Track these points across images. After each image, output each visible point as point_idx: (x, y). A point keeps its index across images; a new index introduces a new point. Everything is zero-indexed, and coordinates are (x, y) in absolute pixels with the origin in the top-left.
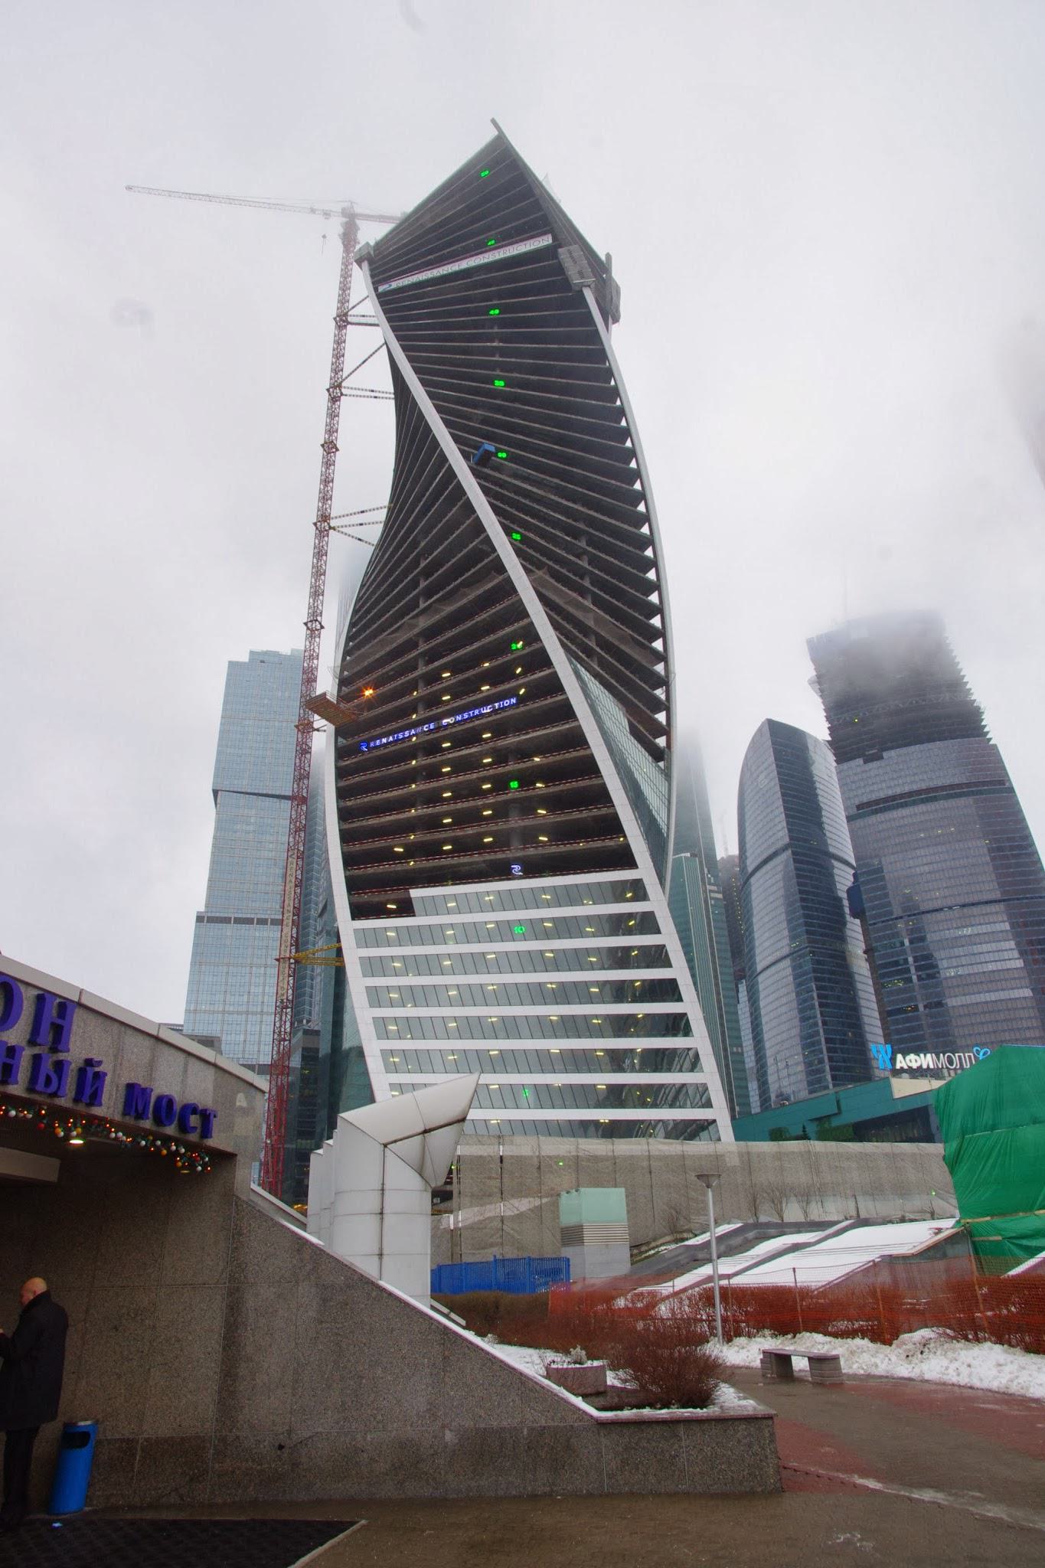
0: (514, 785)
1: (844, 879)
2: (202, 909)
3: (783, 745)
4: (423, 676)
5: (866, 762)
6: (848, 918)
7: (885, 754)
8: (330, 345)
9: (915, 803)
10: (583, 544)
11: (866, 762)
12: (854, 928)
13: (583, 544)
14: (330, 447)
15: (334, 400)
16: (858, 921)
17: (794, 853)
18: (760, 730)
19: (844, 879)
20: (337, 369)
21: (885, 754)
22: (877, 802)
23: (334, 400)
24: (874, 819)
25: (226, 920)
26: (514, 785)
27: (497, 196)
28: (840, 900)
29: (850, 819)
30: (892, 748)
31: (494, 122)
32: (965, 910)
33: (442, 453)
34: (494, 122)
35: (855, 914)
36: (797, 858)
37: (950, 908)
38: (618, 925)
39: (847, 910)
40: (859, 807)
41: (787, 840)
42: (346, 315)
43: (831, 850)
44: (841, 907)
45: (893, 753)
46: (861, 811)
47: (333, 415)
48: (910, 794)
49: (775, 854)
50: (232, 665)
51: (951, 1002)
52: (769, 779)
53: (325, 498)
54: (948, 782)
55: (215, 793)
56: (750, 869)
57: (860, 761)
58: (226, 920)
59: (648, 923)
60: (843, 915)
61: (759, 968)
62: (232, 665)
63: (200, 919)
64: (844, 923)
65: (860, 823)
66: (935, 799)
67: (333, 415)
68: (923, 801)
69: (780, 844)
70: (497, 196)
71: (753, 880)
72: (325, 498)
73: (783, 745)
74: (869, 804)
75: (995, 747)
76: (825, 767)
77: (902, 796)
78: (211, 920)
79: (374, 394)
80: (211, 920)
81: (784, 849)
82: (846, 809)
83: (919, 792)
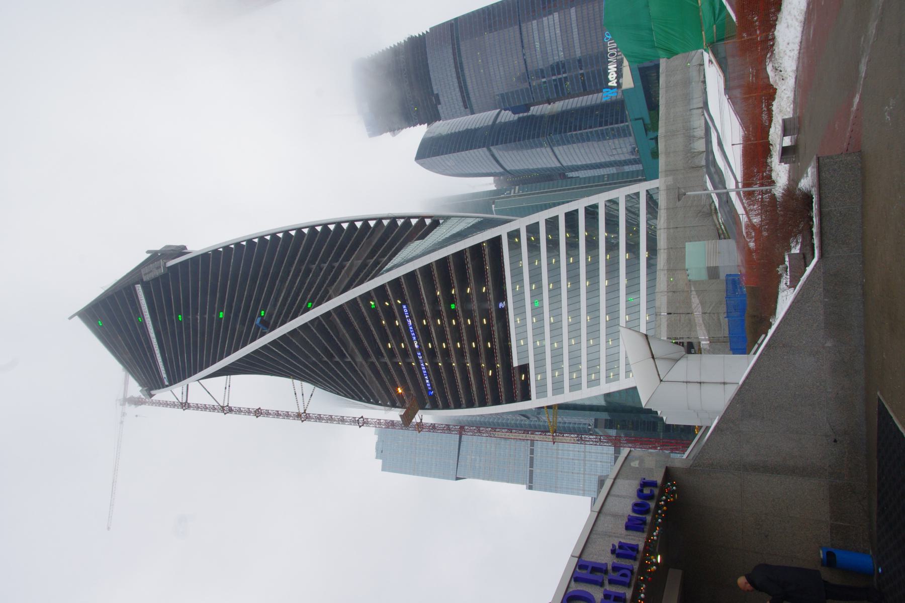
0: (453, 306)
1: (507, 116)
2: (525, 486)
3: (428, 152)
4: (378, 359)
5: (440, 103)
6: (530, 113)
7: (435, 92)
8: (199, 412)
9: (463, 75)
10: (314, 267)
11: (440, 103)
12: (535, 110)
13: (314, 267)
14: (258, 413)
15: (231, 410)
16: (532, 108)
17: (492, 145)
18: (422, 165)
19: (507, 116)
20: (213, 409)
21: (435, 92)
22: (463, 97)
23: (231, 410)
24: (473, 99)
25: (531, 472)
26: (453, 306)
27: (113, 316)
28: (519, 118)
29: (473, 113)
30: (432, 88)
31: (71, 318)
32: (525, 46)
33: (238, 361)
34: (71, 318)
35: (528, 110)
36: (496, 143)
37: (524, 55)
38: (534, 247)
39: (525, 114)
40: (466, 107)
41: (485, 149)
42: (182, 403)
43: (490, 123)
44: (523, 118)
45: (435, 88)
46: (468, 106)
47: (239, 411)
48: (458, 78)
49: (493, 156)
50: (384, 469)
51: (578, 54)
52: (450, 159)
53: (287, 415)
54: (455, 80)
55: (457, 479)
56: (502, 170)
57: (439, 107)
58: (531, 472)
59: (533, 229)
60: (528, 117)
61: (559, 165)
62: (384, 469)
63: (530, 488)
64: (533, 116)
65: (475, 107)
66: (461, 63)
67: (239, 411)
68: (462, 70)
69: (487, 153)
70: (113, 316)
71: (508, 169)
72: (287, 415)
73: (428, 152)
74: (464, 102)
75: (431, 29)
76: (443, 127)
77: (459, 83)
78: (531, 481)
79: (228, 387)
80: (531, 481)
81: (490, 150)
82: (467, 115)
83: (457, 73)
